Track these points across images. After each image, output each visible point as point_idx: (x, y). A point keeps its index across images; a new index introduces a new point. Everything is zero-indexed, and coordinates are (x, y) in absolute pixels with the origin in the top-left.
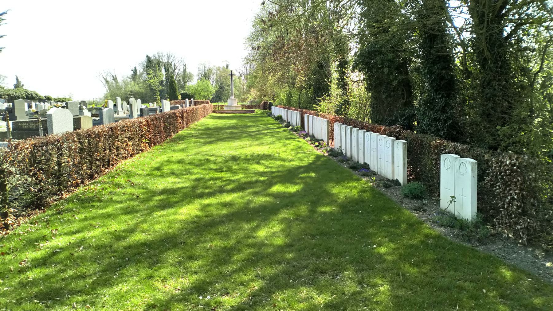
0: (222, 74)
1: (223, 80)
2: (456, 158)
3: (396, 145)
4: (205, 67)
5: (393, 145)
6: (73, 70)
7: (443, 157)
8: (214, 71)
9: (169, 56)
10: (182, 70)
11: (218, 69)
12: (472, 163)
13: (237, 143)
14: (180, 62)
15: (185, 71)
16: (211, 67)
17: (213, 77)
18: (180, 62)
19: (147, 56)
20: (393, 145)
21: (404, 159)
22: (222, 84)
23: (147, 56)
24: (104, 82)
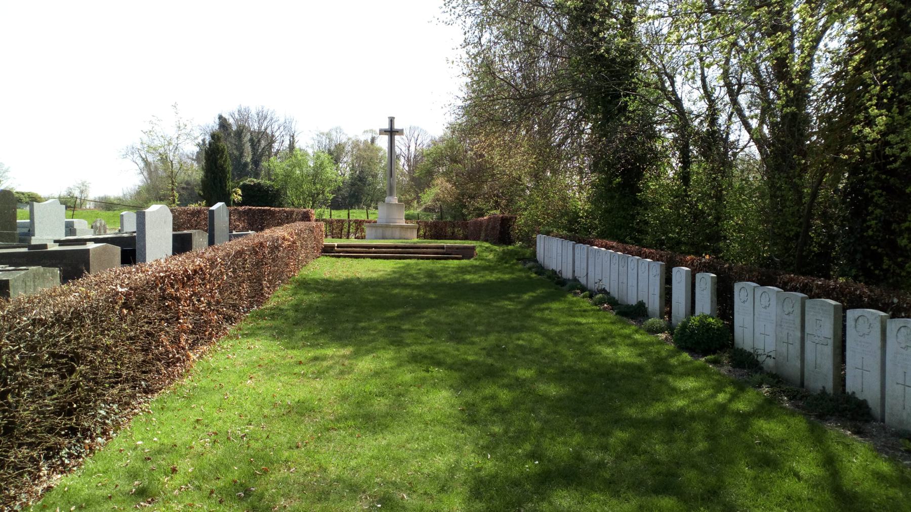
0: (363, 154)
1: (366, 165)
2: (778, 292)
3: (758, 295)
4: (331, 140)
5: (574, 249)
6: (82, 145)
7: (737, 286)
8: (348, 148)
9: (262, 117)
10: (287, 143)
11: (356, 144)
12: (835, 306)
13: (466, 241)
14: (282, 128)
15: (292, 147)
16: (344, 140)
17: (347, 159)
18: (282, 128)
19: (220, 117)
20: (574, 249)
21: (661, 297)
22: (362, 172)
23: (220, 117)
24: (142, 165)
